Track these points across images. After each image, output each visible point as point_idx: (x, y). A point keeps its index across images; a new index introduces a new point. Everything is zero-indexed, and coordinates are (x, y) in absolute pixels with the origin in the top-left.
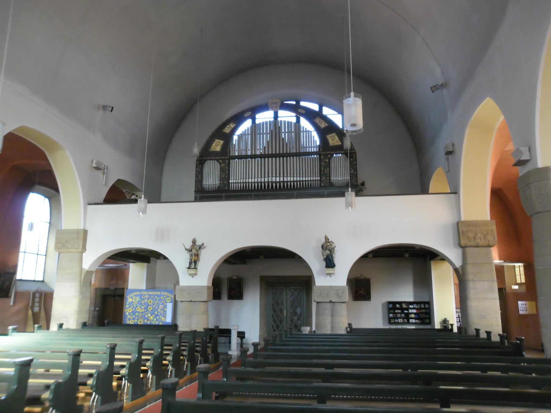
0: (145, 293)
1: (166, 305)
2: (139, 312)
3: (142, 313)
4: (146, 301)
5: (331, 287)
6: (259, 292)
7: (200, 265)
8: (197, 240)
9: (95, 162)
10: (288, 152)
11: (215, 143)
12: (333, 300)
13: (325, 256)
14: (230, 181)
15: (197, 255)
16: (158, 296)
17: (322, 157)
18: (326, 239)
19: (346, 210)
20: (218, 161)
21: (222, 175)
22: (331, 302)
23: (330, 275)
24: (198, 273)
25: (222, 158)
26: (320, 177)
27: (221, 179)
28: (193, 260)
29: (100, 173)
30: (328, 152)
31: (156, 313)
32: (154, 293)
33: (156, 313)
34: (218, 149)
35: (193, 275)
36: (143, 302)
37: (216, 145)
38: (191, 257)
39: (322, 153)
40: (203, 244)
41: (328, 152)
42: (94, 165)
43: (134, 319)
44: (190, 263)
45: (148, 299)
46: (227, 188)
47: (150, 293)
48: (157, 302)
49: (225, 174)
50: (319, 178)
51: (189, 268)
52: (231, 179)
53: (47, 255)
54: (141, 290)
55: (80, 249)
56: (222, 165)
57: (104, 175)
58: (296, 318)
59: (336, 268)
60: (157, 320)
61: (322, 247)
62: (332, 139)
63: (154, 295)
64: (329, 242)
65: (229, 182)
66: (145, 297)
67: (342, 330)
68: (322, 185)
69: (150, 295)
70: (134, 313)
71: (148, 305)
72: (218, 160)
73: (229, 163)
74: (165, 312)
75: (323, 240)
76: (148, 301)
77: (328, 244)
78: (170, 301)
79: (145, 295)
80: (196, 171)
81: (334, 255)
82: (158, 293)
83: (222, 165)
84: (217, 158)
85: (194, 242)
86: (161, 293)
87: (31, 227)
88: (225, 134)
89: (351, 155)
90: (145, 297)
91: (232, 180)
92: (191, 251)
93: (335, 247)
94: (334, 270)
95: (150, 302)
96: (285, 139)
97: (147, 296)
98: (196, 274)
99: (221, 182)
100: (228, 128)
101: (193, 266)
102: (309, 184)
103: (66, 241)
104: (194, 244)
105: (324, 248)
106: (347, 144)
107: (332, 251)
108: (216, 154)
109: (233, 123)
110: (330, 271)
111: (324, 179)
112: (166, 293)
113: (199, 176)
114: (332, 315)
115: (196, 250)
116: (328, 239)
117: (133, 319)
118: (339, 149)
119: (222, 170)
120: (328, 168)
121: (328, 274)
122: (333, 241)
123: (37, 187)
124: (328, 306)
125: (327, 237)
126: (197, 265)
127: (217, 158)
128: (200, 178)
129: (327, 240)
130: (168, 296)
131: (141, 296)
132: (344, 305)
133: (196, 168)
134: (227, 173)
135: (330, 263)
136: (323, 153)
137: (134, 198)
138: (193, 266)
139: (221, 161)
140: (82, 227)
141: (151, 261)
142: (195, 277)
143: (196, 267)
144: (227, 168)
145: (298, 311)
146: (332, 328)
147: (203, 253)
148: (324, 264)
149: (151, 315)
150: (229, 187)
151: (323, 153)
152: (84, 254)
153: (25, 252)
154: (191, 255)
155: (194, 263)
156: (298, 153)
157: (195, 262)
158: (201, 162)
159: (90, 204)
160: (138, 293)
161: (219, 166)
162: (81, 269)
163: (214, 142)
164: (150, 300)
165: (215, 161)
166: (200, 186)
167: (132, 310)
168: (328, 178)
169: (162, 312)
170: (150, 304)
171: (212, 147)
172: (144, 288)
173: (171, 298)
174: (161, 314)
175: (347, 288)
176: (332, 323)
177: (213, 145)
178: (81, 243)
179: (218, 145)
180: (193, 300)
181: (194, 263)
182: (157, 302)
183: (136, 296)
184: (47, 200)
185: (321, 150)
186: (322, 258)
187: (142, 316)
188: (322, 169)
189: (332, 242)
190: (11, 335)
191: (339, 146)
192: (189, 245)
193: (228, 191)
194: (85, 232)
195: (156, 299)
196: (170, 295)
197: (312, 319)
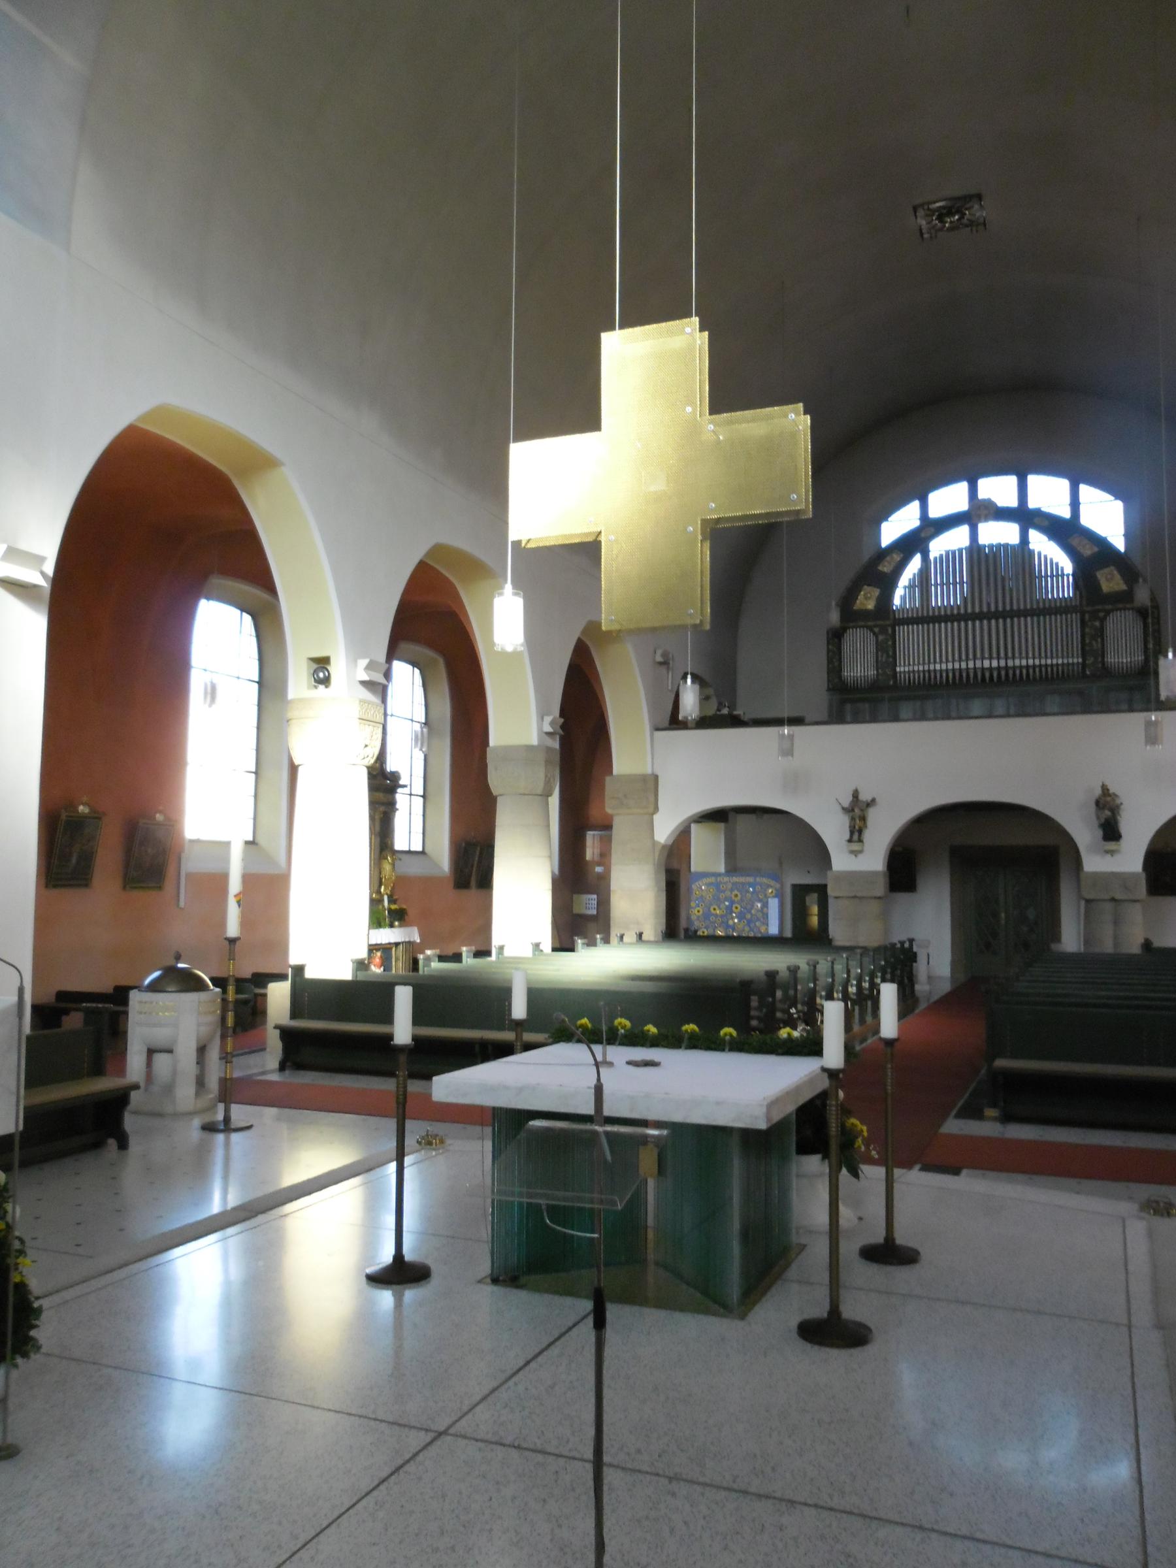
0: (726, 879)
1: (767, 902)
2: (716, 915)
3: (722, 916)
4: (728, 893)
5: (1114, 874)
6: (948, 879)
7: (867, 835)
8: (859, 790)
9: (659, 652)
10: (1015, 607)
11: (862, 593)
12: (1118, 896)
13: (1103, 820)
14: (898, 669)
15: (863, 819)
16: (750, 885)
17: (1087, 616)
18: (1105, 789)
19: (1146, 745)
20: (871, 630)
21: (882, 656)
22: (1113, 900)
23: (1112, 853)
24: (865, 849)
25: (879, 622)
26: (1084, 657)
27: (878, 665)
28: (857, 827)
29: (663, 670)
30: (1100, 607)
31: (748, 916)
32: (742, 879)
33: (748, 916)
34: (871, 605)
35: (855, 853)
36: (722, 896)
37: (866, 598)
38: (853, 822)
39: (1085, 608)
40: (873, 800)
41: (1100, 607)
42: (659, 659)
43: (707, 928)
44: (852, 833)
45: (732, 890)
46: (891, 683)
47: (735, 879)
48: (749, 895)
49: (887, 652)
50: (1080, 660)
51: (850, 841)
52: (898, 664)
53: (427, 794)
54: (719, 875)
55: (651, 810)
56: (881, 638)
57: (668, 673)
58: (1025, 929)
59: (1124, 842)
60: (751, 930)
61: (1097, 803)
62: (1107, 580)
63: (743, 884)
64: (1109, 795)
65: (895, 670)
66: (727, 888)
67: (1134, 946)
68: (1088, 673)
69: (734, 884)
70: (707, 915)
71: (732, 902)
72: (871, 629)
73: (894, 631)
74: (766, 916)
75: (1098, 792)
76: (731, 893)
77: (1109, 799)
78: (774, 894)
79: (726, 883)
80: (828, 651)
81: (1119, 818)
82: (751, 879)
83: (881, 638)
84: (870, 623)
85: (856, 794)
86: (755, 880)
87: (212, 693)
88: (884, 574)
89: (1150, 617)
90: (727, 888)
91: (900, 665)
92: (853, 810)
93: (1122, 804)
94: (1120, 845)
95: (736, 896)
96: (998, 554)
97: (730, 886)
98: (861, 852)
99: (880, 671)
100: (889, 563)
101: (856, 837)
102: (1060, 672)
103: (625, 796)
104: (855, 799)
105: (1101, 806)
106: (1142, 596)
107: (1115, 810)
108: (865, 615)
109: (899, 552)
110: (1111, 845)
111: (1090, 661)
112: (765, 880)
113: (834, 660)
114: (1116, 922)
115: (862, 810)
116: (1108, 790)
117: (705, 928)
118: (1123, 599)
119: (880, 647)
120: (1099, 640)
121: (1107, 852)
122: (1117, 793)
123: (216, 581)
124: (1108, 906)
125: (1107, 786)
126: (862, 835)
127: (870, 623)
128: (836, 664)
129: (1106, 791)
130: (769, 886)
131: (717, 886)
132: (1138, 906)
133: (828, 643)
134: (891, 653)
135: (1111, 832)
136: (1089, 609)
137: (727, 712)
138: (856, 837)
139: (876, 630)
140: (649, 771)
141: (730, 819)
142: (860, 856)
143: (861, 838)
144: (890, 643)
145: (1031, 914)
146: (1116, 945)
147: (872, 814)
148: (1100, 833)
149: (739, 921)
150: (895, 682)
151: (1089, 609)
152: (656, 817)
153: (411, 795)
154: (853, 819)
155: (857, 833)
156: (1035, 610)
157: (860, 832)
158: (836, 637)
159: (658, 729)
160: (712, 880)
161: (873, 638)
162: (654, 843)
163: (860, 591)
164: (736, 892)
165: (865, 629)
166: (836, 680)
167: (703, 911)
168: (1100, 659)
169: (760, 915)
170: (736, 899)
171: (858, 602)
172: (723, 870)
173: (776, 890)
174: (758, 919)
175: (1144, 876)
176: (1116, 937)
177: (859, 597)
178: (652, 799)
179: (870, 598)
180: (859, 894)
181: (857, 833)
182: (749, 895)
183: (711, 884)
184: (247, 618)
185: (1084, 602)
186: (1096, 823)
187: (723, 922)
188: (1087, 641)
189: (1116, 796)
190: (600, 946)
191: (1124, 592)
192: (847, 801)
193: (896, 687)
194: (656, 777)
195: (748, 891)
196: (772, 883)
197: (355, 1032)
